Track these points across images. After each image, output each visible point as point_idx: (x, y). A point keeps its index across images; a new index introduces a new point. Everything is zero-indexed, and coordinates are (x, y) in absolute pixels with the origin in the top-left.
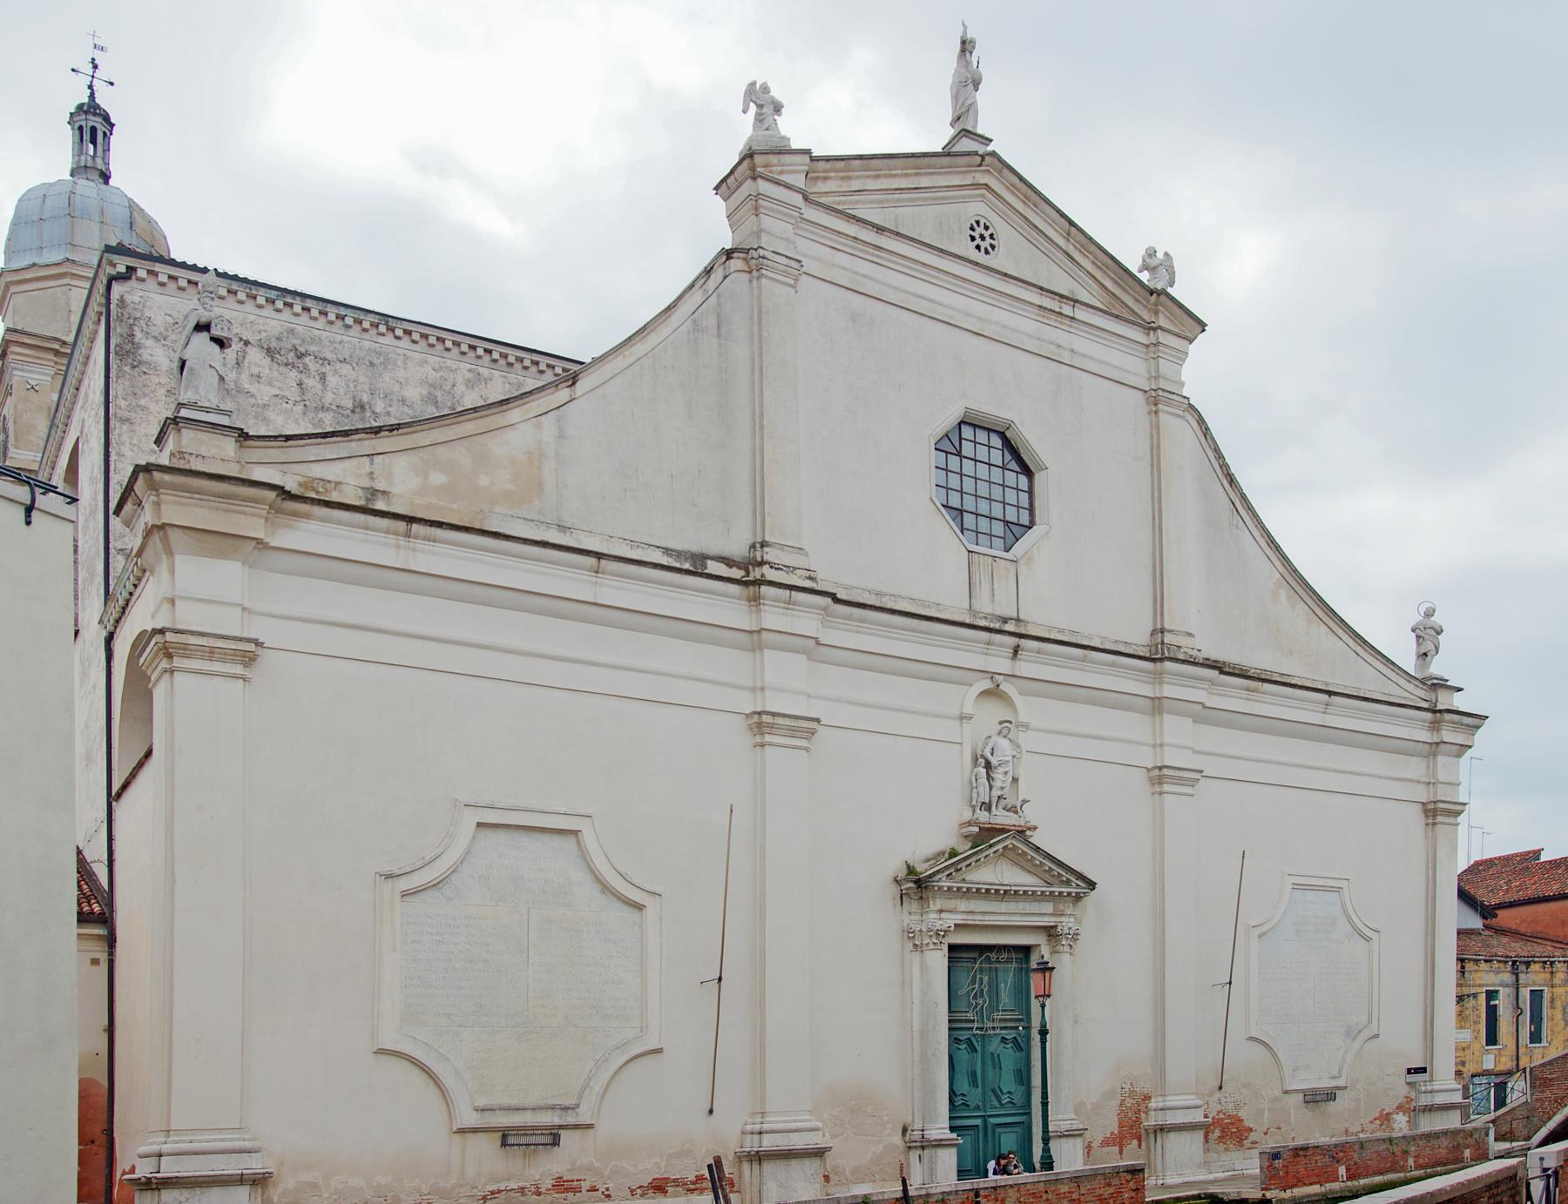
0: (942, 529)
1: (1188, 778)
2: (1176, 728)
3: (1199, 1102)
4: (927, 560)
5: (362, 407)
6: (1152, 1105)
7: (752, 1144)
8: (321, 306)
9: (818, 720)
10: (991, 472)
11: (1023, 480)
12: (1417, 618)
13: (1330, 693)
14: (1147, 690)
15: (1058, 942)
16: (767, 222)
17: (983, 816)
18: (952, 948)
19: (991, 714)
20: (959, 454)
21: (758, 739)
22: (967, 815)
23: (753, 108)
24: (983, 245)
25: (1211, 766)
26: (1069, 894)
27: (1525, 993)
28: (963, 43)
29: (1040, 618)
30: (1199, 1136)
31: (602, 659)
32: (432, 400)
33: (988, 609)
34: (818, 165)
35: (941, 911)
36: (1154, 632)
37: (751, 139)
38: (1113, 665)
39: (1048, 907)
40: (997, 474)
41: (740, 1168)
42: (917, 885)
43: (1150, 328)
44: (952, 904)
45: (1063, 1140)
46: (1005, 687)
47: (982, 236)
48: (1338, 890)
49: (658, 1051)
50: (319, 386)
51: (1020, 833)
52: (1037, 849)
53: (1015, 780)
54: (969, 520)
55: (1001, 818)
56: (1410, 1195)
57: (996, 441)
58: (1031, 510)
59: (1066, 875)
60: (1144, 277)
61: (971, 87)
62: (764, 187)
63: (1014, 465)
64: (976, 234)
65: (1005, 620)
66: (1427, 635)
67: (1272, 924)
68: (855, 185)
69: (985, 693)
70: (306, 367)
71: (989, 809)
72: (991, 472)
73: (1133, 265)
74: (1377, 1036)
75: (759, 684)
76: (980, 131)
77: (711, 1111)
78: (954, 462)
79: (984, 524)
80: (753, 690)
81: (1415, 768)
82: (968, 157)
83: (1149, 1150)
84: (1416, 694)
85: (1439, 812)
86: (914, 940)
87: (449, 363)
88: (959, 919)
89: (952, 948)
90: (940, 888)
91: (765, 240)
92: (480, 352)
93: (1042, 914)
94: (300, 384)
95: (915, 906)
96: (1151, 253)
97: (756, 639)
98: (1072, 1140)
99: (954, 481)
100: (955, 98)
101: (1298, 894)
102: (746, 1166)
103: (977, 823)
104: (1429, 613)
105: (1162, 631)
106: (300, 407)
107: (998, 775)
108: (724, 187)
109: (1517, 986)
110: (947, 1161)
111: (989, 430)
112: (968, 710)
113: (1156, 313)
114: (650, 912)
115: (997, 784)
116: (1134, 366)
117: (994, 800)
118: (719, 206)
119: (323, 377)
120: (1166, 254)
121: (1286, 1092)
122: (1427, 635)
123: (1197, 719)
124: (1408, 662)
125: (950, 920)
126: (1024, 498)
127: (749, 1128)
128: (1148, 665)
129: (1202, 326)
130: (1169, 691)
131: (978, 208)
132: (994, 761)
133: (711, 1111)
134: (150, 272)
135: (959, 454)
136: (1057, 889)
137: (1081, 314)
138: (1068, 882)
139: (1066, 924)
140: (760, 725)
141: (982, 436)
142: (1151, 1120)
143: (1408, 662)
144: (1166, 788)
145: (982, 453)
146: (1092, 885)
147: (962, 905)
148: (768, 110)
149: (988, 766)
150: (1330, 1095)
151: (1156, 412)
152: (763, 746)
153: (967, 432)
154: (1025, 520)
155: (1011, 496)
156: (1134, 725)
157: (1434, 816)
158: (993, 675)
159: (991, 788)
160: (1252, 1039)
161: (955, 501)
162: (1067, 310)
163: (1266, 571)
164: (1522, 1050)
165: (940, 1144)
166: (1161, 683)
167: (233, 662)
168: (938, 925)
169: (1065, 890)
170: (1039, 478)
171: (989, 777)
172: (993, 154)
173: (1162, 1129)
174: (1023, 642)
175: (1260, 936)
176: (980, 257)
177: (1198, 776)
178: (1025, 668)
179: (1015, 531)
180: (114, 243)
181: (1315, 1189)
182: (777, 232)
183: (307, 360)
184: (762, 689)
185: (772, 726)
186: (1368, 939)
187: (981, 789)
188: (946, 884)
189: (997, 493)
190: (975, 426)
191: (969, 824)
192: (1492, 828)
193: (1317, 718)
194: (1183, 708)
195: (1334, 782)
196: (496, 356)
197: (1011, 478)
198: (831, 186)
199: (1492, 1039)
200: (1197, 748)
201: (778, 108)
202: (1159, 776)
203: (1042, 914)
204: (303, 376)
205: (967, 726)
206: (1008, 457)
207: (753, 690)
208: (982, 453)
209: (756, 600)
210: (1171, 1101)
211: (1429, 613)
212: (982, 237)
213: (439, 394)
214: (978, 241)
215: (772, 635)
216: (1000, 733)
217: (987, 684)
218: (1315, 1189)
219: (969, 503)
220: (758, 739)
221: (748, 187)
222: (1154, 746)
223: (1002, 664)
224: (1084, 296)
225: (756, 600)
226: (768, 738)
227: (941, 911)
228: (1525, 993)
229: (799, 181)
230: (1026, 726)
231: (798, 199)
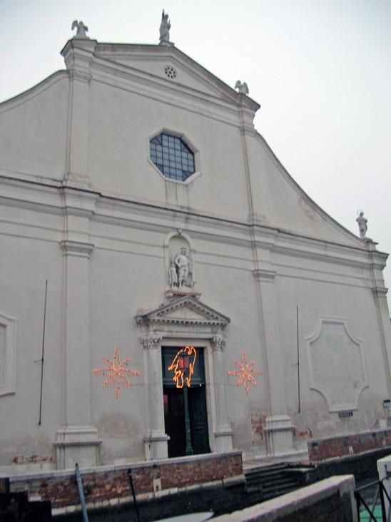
0: (154, 171)
1: (271, 276)
2: (262, 254)
4: (150, 185)
6: (267, 420)
7: (60, 440)
10: (173, 153)
11: (190, 156)
12: (357, 216)
13: (326, 242)
14: (248, 238)
15: (215, 345)
16: (77, 61)
17: (175, 289)
18: (163, 348)
19: (177, 246)
20: (161, 145)
21: (65, 253)
22: (168, 288)
23: (76, 29)
25: (279, 270)
26: (218, 324)
28: (163, 14)
29: (198, 207)
30: (290, 434)
33: (175, 203)
34: (99, 46)
35: (155, 331)
36: (249, 216)
37: (74, 37)
38: (232, 227)
39: (209, 330)
40: (178, 153)
41: (56, 453)
42: (144, 320)
43: (239, 106)
44: (161, 327)
45: (222, 438)
46: (184, 234)
47: (170, 71)
48: (342, 324)
49: (13, 394)
51: (194, 296)
52: (200, 304)
53: (190, 274)
54: (166, 169)
55: (183, 289)
57: (179, 142)
58: (194, 167)
59: (215, 315)
60: (237, 90)
61: (166, 28)
62: (76, 50)
63: (186, 150)
65: (182, 207)
66: (362, 222)
67: (316, 337)
69: (174, 237)
71: (178, 285)
72: (173, 153)
73: (232, 85)
74: (367, 387)
75: (65, 229)
77: (40, 423)
78: (159, 148)
79: (173, 171)
80: (63, 232)
81: (366, 274)
82: (165, 46)
83: (266, 440)
84: (362, 245)
86: (145, 345)
88: (165, 334)
89: (163, 348)
90: (154, 320)
91: (76, 68)
93: (206, 333)
95: (144, 328)
96: (239, 82)
97: (65, 211)
98: (226, 438)
99: (159, 155)
100: (161, 31)
101: (325, 325)
102: (58, 450)
103: (172, 292)
104: (362, 214)
105: (253, 215)
107: (182, 271)
108: (63, 52)
110: (163, 448)
111: (174, 137)
112: (167, 243)
113: (241, 101)
114: (9, 329)
115: (181, 275)
116: (234, 119)
117: (181, 282)
118: (62, 58)
120: (245, 83)
121: (331, 413)
122: (362, 222)
123: (272, 250)
124: (357, 232)
125: (160, 335)
126: (191, 163)
127: (59, 431)
128: (248, 228)
129: (259, 106)
130: (257, 238)
131: (170, 64)
132: (179, 265)
133: (40, 423)
135: (161, 145)
136: (212, 322)
137: (210, 99)
138: (217, 318)
139: (219, 337)
140: (65, 247)
142: (267, 427)
143: (357, 232)
144: (261, 279)
145: (172, 145)
146: (228, 320)
147: (166, 328)
148: (81, 29)
149: (177, 268)
150: (350, 414)
151: (244, 135)
152: (67, 255)
153: (165, 137)
154: (191, 169)
155: (185, 161)
156: (245, 252)
157: (377, 293)
158: (177, 229)
159: (178, 276)
160: (312, 389)
161: (160, 161)
162: (206, 98)
163: (295, 195)
165: (158, 440)
166: (254, 235)
167: (85, 252)
168: (154, 337)
169: (216, 322)
170: (196, 155)
171: (177, 272)
173: (271, 431)
174: (189, 216)
175: (311, 343)
178: (192, 227)
179: (186, 174)
182: (82, 66)
184: (67, 231)
185: (71, 247)
186: (358, 345)
187: (173, 277)
188: (157, 318)
189: (179, 160)
190: (168, 135)
191: (168, 292)
193: (322, 252)
194: (265, 246)
195: (320, 276)
197: (184, 155)
200: (273, 262)
201: (86, 29)
202: (257, 274)
203: (206, 333)
205: (167, 251)
206: (183, 147)
207: (63, 232)
208: (172, 145)
209: (63, 195)
210: (275, 418)
211: (362, 214)
215: (70, 209)
216: (181, 253)
217: (175, 233)
219: (166, 163)
220: (65, 253)
221: (71, 51)
222: (254, 261)
223: (180, 225)
224: (212, 93)
225: (63, 195)
226: (69, 252)
227: (155, 331)
229: (92, 49)
230: (195, 252)
231: (91, 55)
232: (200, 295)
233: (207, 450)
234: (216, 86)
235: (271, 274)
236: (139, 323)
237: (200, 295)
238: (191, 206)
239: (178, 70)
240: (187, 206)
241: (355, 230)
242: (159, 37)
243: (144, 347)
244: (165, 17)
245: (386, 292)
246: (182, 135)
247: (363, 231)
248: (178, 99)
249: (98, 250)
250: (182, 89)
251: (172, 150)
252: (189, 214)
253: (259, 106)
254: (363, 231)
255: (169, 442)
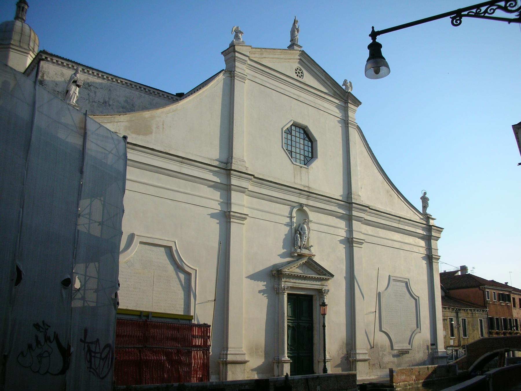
0: (284, 157)
3: (367, 352)
5: (106, 102)
8: (140, 85)
9: (248, 215)
24: (299, 75)
27: (460, 320)
28: (295, 21)
31: (139, 180)
32: (126, 101)
33: (299, 182)
40: (302, 141)
46: (305, 208)
50: (94, 95)
54: (294, 154)
56: (469, 384)
57: (302, 131)
60: (344, 87)
63: (307, 139)
64: (297, 72)
66: (425, 200)
68: (264, 56)
70: (91, 89)
73: (341, 83)
76: (298, 44)
85: (430, 258)
87: (133, 91)
92: (142, 89)
94: (88, 94)
104: (425, 193)
106: (87, 101)
109: (457, 317)
118: (222, 57)
119: (95, 93)
122: (425, 200)
126: (310, 149)
134: (51, 59)
141: (298, 129)
153: (293, 128)
161: (289, 149)
164: (461, 339)
172: (303, 51)
176: (298, 78)
177: (363, 241)
178: (311, 203)
180: (42, 50)
181: (512, 365)
183: (92, 87)
192: (448, 263)
196: (147, 90)
197: (306, 142)
198: (256, 55)
199: (452, 335)
204: (89, 92)
206: (305, 136)
211: (425, 193)
212: (299, 73)
213: (128, 100)
214: (298, 74)
218: (512, 365)
219: (294, 150)
223: (303, 201)
228: (460, 320)
232: (315, 255)
233: (210, 326)
234: (330, 85)
235: (361, 241)
236: (273, 276)
237: (315, 255)
238: (310, 186)
239: (305, 72)
240: (307, 185)
241: (419, 206)
242: (479, 271)
243: (277, 293)
244: (295, 22)
245: (439, 259)
246: (306, 127)
247: (425, 207)
248: (304, 96)
249: (216, 198)
250: (306, 88)
251: (300, 142)
252: (309, 194)
253: (360, 103)
254: (425, 207)
255: (291, 363)
